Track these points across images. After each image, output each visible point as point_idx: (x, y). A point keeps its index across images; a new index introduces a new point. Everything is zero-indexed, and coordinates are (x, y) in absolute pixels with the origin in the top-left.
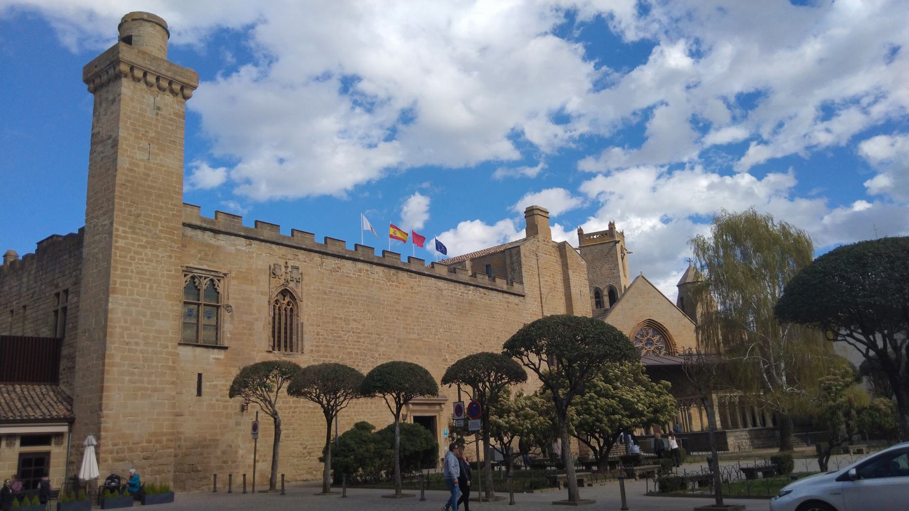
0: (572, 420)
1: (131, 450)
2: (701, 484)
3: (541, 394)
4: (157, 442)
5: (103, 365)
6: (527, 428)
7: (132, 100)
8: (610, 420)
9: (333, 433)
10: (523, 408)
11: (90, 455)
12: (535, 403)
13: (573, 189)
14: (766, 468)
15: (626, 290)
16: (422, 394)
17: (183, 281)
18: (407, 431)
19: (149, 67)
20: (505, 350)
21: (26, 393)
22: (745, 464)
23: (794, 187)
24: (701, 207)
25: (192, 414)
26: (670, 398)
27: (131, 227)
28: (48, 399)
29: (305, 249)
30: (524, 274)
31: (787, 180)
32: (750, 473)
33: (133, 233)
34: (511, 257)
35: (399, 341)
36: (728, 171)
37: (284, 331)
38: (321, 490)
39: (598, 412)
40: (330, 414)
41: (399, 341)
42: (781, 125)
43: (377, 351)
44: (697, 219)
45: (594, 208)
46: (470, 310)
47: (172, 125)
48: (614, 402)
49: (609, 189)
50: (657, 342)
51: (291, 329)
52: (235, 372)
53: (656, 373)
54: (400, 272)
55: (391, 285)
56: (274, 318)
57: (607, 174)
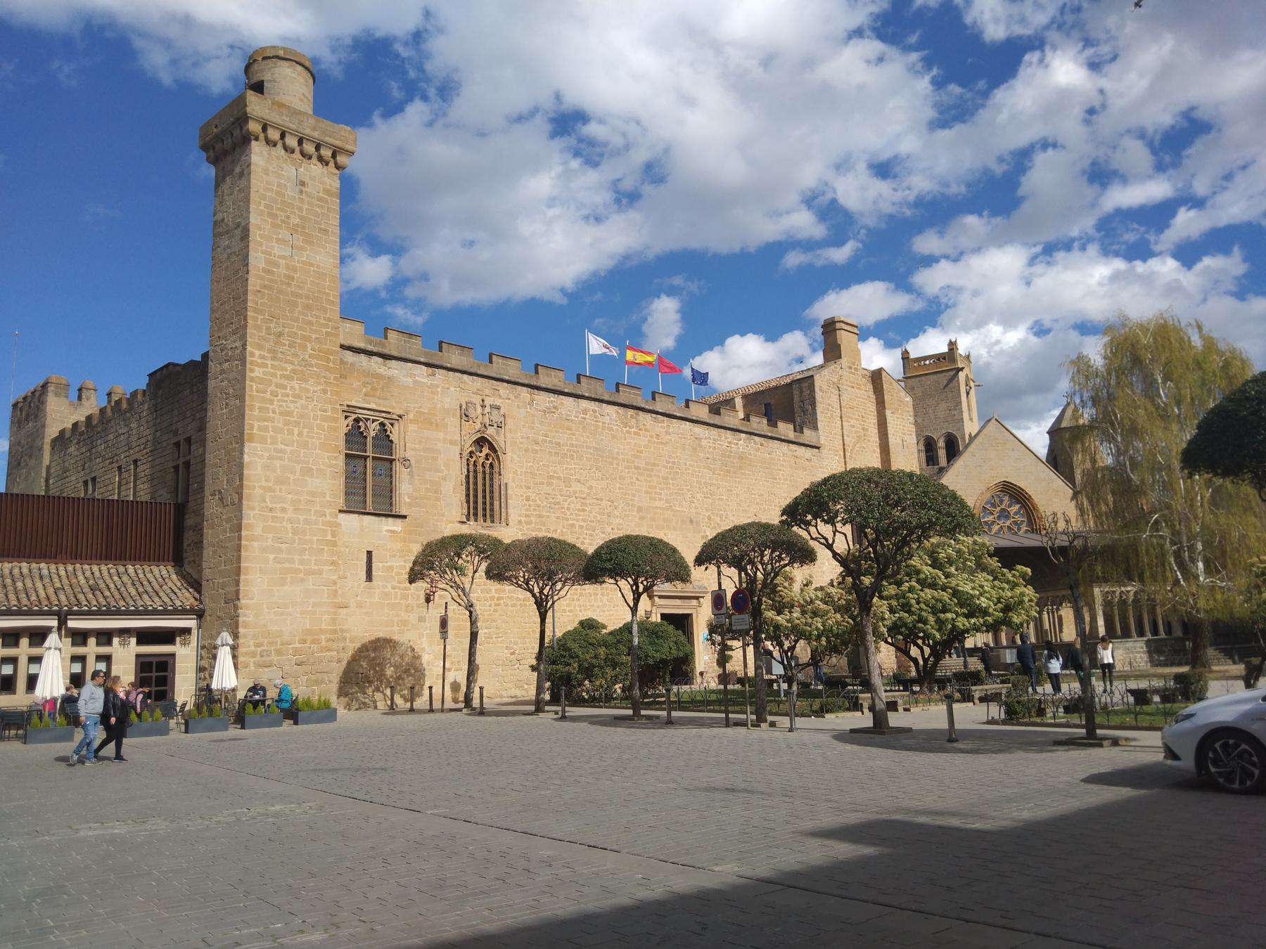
0: (883, 619)
1: (279, 652)
2: (1068, 710)
3: (839, 583)
4: (314, 642)
5: (240, 538)
6: (817, 629)
7: (266, 172)
8: (938, 621)
9: (548, 633)
10: (812, 602)
11: (224, 655)
12: (829, 595)
13: (902, 283)
14: (1166, 689)
15: (972, 439)
16: (669, 580)
17: (343, 426)
18: (649, 631)
19: (287, 124)
20: (784, 518)
21: (141, 576)
22: (1133, 685)
23: (1244, 276)
24: (1097, 309)
25: (360, 605)
26: (1029, 591)
27: (270, 351)
28: (170, 584)
29: (508, 382)
30: (819, 416)
31: (1231, 265)
32: (1141, 696)
33: (274, 358)
34: (801, 392)
35: (640, 509)
36: (1140, 252)
37: (482, 493)
38: (533, 708)
39: (921, 609)
40: (543, 606)
41: (640, 509)
42: (1228, 177)
43: (609, 524)
44: (1085, 328)
45: (932, 314)
46: (740, 468)
47: (322, 207)
48: (945, 596)
49: (957, 282)
50: (1016, 513)
51: (492, 492)
52: (416, 549)
53: (1008, 557)
54: (641, 413)
55: (629, 432)
56: (468, 477)
57: (956, 258)
